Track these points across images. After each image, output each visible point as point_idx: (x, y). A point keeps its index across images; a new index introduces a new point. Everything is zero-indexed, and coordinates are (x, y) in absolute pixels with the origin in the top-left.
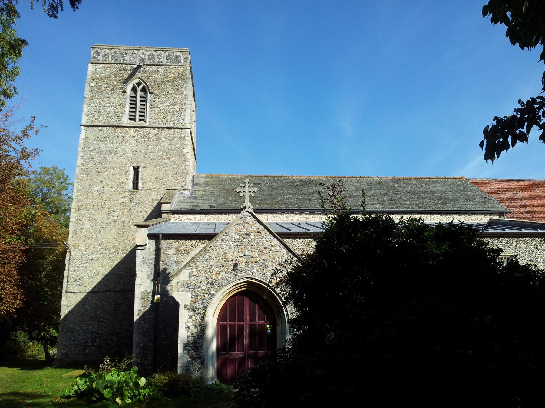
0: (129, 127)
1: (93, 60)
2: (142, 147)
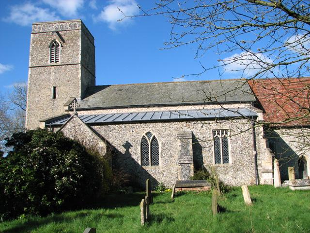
0: (51, 66)
1: (33, 32)
2: (57, 76)
